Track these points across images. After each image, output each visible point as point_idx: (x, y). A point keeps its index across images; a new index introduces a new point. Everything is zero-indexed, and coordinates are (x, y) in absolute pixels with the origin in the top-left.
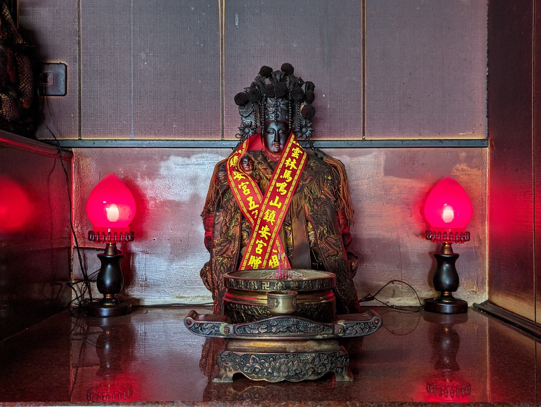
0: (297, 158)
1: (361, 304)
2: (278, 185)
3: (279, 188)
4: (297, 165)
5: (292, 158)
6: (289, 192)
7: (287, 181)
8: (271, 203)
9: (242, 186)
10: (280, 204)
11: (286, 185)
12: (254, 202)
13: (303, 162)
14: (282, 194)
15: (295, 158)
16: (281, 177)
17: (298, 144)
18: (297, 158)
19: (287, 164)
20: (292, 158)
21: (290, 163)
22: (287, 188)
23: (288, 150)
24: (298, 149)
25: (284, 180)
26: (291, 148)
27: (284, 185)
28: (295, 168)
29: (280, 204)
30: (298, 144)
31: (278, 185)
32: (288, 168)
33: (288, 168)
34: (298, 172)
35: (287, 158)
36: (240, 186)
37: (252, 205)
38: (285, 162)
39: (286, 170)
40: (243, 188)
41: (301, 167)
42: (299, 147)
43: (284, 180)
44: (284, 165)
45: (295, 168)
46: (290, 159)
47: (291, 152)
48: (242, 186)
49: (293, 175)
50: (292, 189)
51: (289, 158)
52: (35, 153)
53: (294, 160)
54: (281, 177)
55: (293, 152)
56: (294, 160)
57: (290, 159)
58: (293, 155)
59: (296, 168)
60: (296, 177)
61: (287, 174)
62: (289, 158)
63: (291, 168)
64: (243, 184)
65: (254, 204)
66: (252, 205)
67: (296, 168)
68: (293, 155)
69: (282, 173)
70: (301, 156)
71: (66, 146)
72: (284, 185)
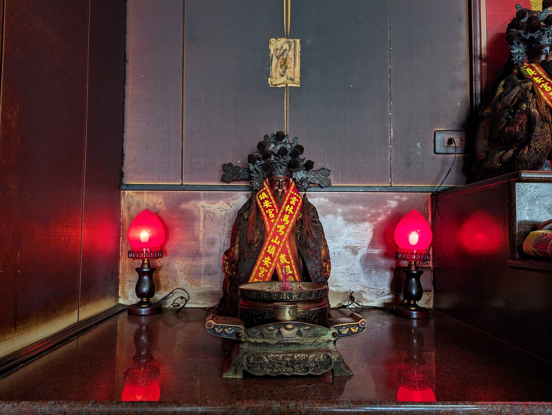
2: (278, 226)
4: (294, 211)
5: (291, 205)
10: (279, 241)
13: (298, 208)
15: (293, 205)
20: (291, 205)
22: (285, 230)
26: (290, 197)
27: (282, 227)
28: (292, 213)
29: (279, 241)
31: (278, 226)
35: (286, 205)
42: (296, 196)
45: (292, 213)
47: (290, 200)
53: (292, 207)
56: (292, 207)
58: (291, 203)
68: (291, 203)
69: (282, 217)
70: (297, 203)
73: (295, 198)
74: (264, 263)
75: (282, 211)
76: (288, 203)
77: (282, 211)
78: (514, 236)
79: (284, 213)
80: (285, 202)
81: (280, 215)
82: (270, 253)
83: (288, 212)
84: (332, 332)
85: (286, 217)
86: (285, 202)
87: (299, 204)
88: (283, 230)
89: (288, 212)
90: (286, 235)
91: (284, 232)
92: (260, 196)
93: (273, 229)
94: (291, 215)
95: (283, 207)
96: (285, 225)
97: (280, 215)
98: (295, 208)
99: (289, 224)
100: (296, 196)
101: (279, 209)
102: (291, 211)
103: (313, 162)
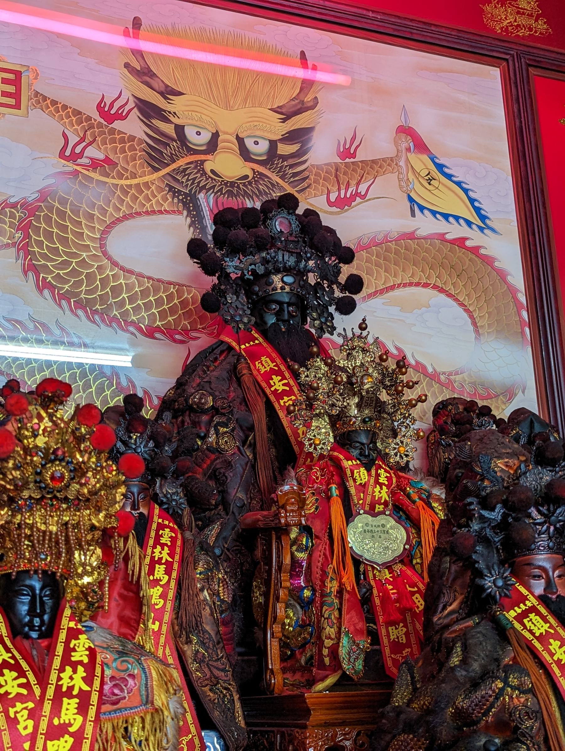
0: (169, 544)
4: (89, 680)
5: (74, 665)
6: (168, 602)
7: (161, 583)
9: (16, 712)
10: (157, 623)
11: (161, 589)
13: (178, 550)
14: (157, 607)
15: (81, 663)
16: (56, 722)
17: (166, 522)
18: (169, 544)
19: (65, 683)
20: (163, 546)
21: (71, 678)
22: (163, 596)
23: (60, 649)
24: (167, 530)
25: (156, 582)
26: (157, 531)
28: (86, 688)
29: (157, 623)
30: (166, 522)
32: (159, 561)
33: (159, 561)
34: (176, 566)
36: (12, 712)
39: (65, 700)
40: (18, 716)
41: (177, 557)
42: (168, 527)
43: (156, 582)
44: (152, 558)
45: (86, 688)
46: (69, 669)
47: (158, 537)
48: (16, 712)
49: (168, 572)
50: (171, 595)
51: (158, 546)
53: (80, 669)
54: (56, 722)
55: (74, 650)
56: (80, 669)
57: (69, 669)
59: (88, 689)
60: (174, 574)
61: (160, 571)
62: (158, 546)
63: (75, 692)
64: (19, 706)
67: (88, 689)
68: (163, 541)
69: (151, 571)
70: (173, 540)
73: (167, 530)
74: (276, 390)
75: (50, 692)
76: (67, 661)
77: (50, 692)
79: (61, 695)
80: (57, 662)
81: (47, 707)
83: (71, 688)
86: (57, 662)
87: (179, 543)
88: (160, 597)
89: (71, 688)
90: (169, 606)
91: (162, 602)
94: (84, 697)
95: (53, 677)
96: (71, 735)
97: (47, 707)
98: (172, 548)
99: (169, 581)
100: (168, 527)
101: (43, 682)
102: (79, 684)
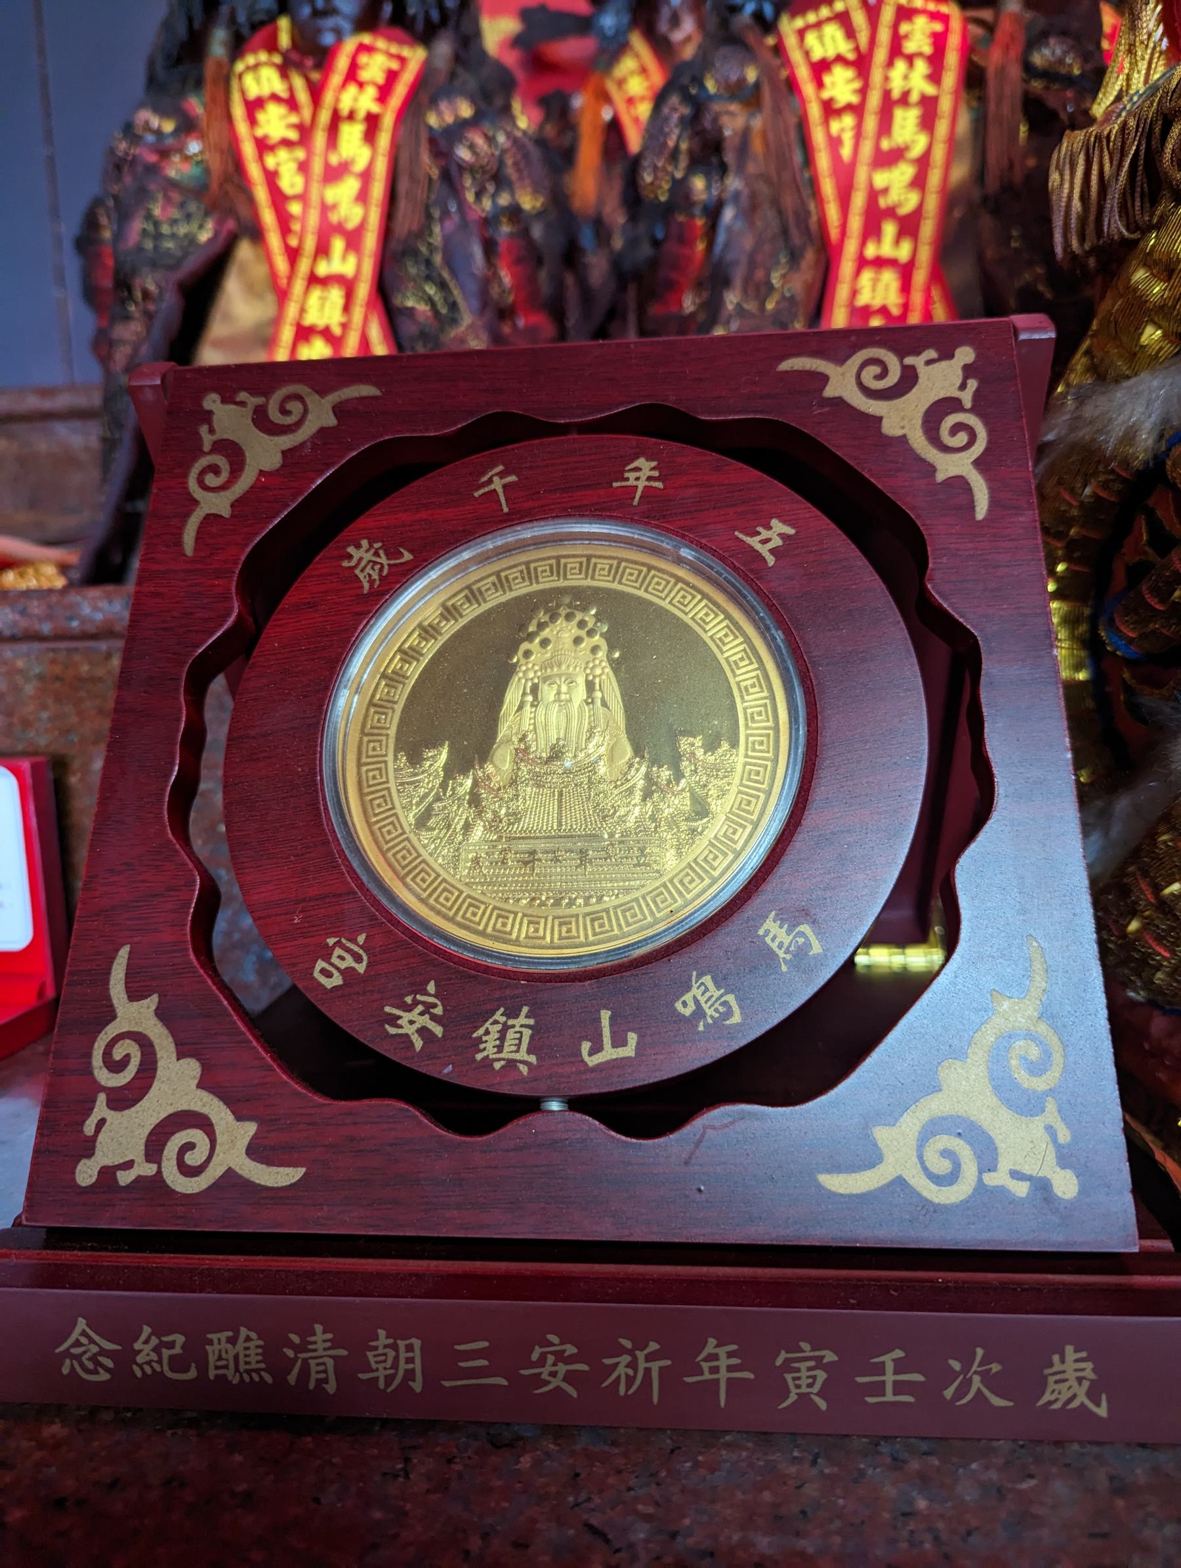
1: (389, 1390)
2: (881, 179)
3: (885, 191)
4: (935, 77)
5: (910, 59)
8: (871, 251)
10: (626, 475)
12: (777, 542)
15: (920, 54)
16: (885, 145)
23: (884, 35)
26: (895, 27)
27: (903, 173)
31: (881, 179)
35: (890, 64)
37: (765, 542)
38: (887, 79)
52: (321, 1205)
57: (900, 66)
58: (910, 47)
65: (771, 545)
66: (765, 542)
70: (939, 41)
71: (605, 1231)
72: (903, 173)
76: (896, 50)
78: (1144, 1255)
82: (877, 303)
83: (906, 95)
84: (145, 226)
85: (906, 123)
89: (906, 95)
92: (811, 39)
93: (858, 201)
103: (200, 1086)
